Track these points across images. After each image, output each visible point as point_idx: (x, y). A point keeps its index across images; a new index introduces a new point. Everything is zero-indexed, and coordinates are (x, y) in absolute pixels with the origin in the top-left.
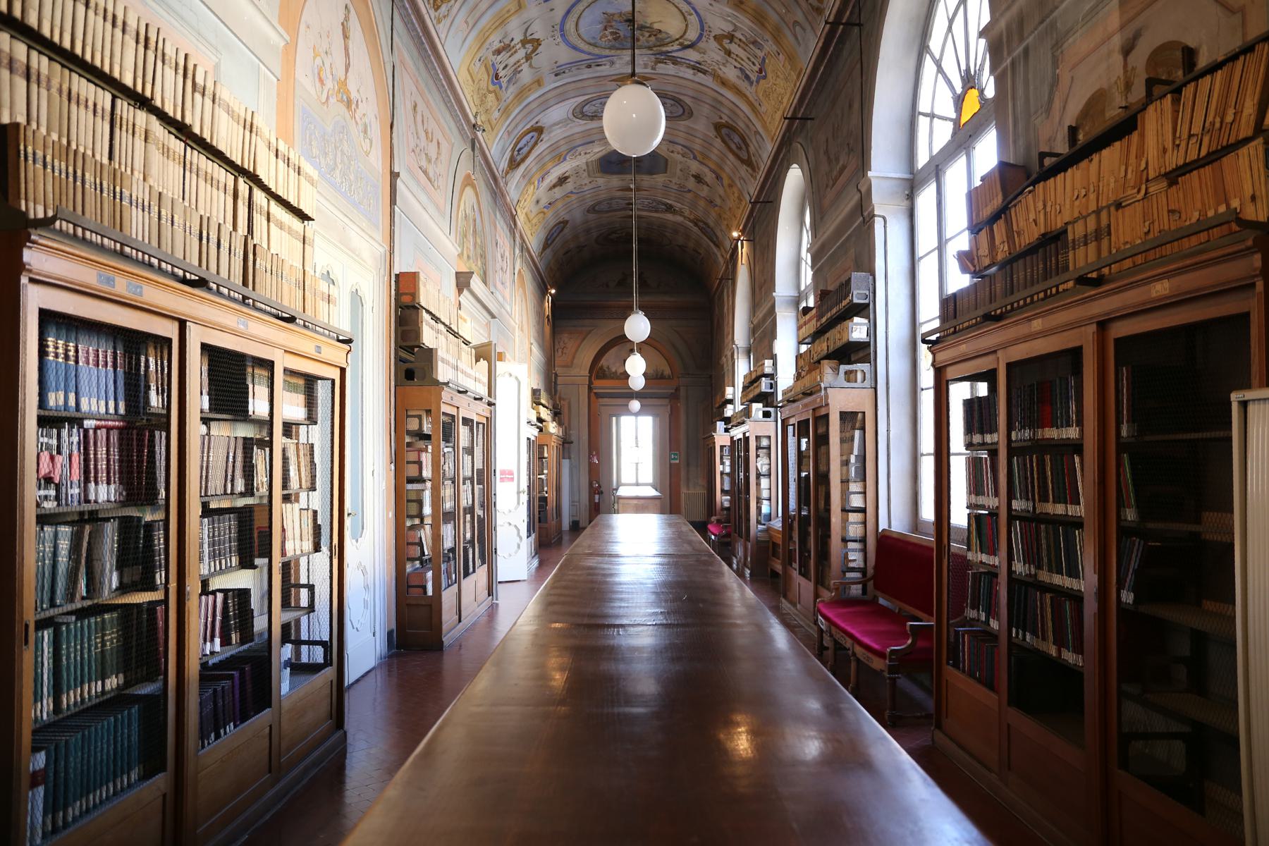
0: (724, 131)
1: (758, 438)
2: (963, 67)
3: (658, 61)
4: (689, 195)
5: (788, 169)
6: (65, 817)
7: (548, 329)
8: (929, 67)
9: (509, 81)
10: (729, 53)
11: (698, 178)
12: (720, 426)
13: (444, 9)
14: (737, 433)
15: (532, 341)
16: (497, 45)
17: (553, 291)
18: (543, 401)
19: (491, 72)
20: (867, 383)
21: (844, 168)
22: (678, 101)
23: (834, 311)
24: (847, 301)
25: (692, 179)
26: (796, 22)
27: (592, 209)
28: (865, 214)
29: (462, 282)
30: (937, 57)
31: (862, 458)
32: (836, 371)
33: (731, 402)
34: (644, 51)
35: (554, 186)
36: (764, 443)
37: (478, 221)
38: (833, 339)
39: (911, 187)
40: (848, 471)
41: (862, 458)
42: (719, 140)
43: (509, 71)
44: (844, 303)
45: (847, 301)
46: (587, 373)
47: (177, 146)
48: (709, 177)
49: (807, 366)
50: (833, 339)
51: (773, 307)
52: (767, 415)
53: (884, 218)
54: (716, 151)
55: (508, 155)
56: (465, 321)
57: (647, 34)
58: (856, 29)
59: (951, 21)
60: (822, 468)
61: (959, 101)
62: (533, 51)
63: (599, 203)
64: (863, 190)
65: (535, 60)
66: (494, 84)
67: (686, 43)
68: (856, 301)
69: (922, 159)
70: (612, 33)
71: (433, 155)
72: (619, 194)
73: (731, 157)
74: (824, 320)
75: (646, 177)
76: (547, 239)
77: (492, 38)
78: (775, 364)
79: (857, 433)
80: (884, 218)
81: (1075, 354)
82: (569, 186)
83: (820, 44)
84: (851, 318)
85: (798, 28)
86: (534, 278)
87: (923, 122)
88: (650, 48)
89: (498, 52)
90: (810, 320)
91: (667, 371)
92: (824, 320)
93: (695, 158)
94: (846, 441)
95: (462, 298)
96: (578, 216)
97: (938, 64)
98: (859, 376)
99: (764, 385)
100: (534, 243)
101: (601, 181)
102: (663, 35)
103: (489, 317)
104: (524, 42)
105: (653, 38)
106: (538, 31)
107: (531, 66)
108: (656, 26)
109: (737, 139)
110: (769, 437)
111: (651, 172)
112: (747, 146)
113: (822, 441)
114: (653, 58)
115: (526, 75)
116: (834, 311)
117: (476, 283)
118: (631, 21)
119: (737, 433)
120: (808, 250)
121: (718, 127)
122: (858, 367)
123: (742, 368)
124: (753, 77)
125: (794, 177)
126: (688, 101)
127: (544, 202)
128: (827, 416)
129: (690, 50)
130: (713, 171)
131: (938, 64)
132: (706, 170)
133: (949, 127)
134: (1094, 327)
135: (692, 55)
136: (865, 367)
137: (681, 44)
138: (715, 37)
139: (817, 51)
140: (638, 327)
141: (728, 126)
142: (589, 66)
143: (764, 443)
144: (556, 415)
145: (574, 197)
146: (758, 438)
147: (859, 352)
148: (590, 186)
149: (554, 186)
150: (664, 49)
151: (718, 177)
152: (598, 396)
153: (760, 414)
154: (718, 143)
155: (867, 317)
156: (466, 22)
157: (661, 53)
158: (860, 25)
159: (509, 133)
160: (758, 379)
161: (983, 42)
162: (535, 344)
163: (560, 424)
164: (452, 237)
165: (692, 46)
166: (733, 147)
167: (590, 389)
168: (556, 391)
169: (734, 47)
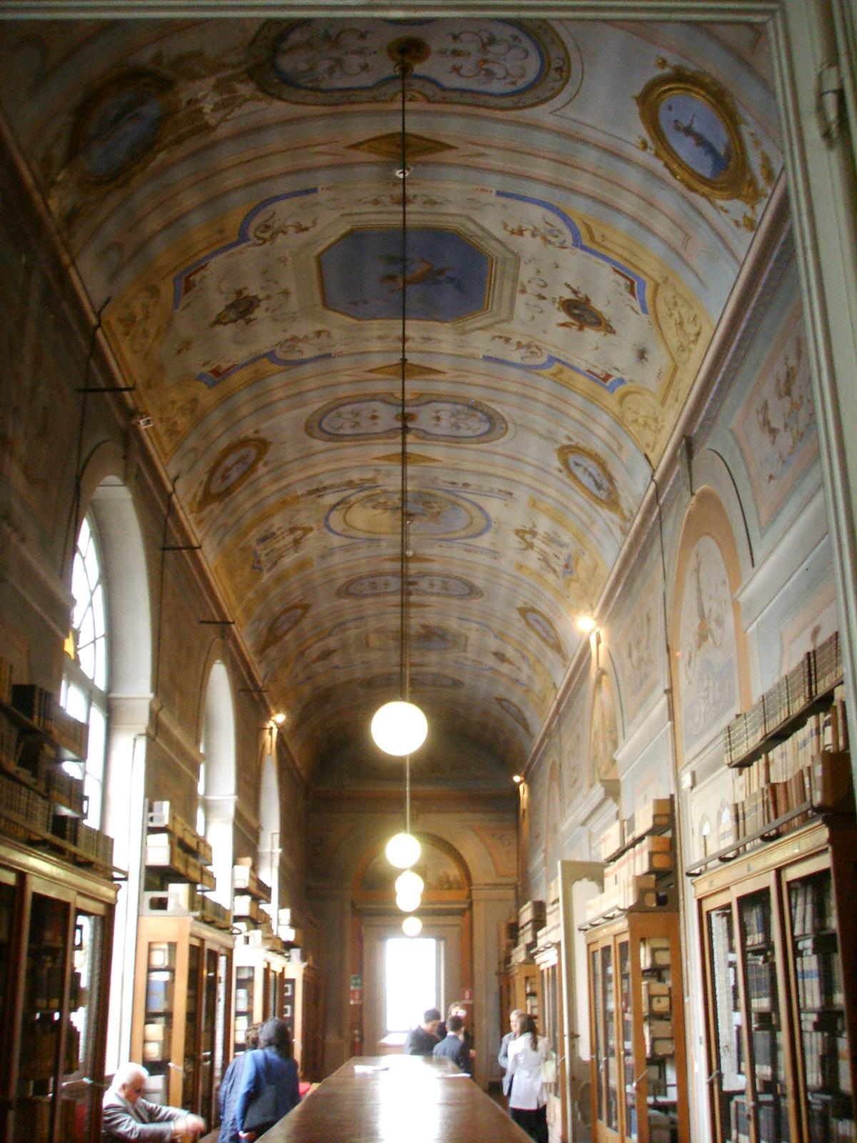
0: (252, 452)
3: (373, 480)
5: (210, 667)
6: (820, 913)
22: (335, 437)
34: (391, 489)
47: (609, 184)
60: (346, 438)
67: (340, 507)
70: (432, 508)
72: (449, 126)
81: (766, 891)
88: (385, 492)
93: (271, 355)
101: (491, 221)
102: (370, 504)
104: (530, 546)
106: (514, 541)
108: (379, 511)
114: (380, 482)
118: (407, 515)
126: (319, 444)
134: (773, 873)
135: (330, 499)
142: (465, 485)
152: (461, 912)
157: (370, 488)
165: (333, 507)
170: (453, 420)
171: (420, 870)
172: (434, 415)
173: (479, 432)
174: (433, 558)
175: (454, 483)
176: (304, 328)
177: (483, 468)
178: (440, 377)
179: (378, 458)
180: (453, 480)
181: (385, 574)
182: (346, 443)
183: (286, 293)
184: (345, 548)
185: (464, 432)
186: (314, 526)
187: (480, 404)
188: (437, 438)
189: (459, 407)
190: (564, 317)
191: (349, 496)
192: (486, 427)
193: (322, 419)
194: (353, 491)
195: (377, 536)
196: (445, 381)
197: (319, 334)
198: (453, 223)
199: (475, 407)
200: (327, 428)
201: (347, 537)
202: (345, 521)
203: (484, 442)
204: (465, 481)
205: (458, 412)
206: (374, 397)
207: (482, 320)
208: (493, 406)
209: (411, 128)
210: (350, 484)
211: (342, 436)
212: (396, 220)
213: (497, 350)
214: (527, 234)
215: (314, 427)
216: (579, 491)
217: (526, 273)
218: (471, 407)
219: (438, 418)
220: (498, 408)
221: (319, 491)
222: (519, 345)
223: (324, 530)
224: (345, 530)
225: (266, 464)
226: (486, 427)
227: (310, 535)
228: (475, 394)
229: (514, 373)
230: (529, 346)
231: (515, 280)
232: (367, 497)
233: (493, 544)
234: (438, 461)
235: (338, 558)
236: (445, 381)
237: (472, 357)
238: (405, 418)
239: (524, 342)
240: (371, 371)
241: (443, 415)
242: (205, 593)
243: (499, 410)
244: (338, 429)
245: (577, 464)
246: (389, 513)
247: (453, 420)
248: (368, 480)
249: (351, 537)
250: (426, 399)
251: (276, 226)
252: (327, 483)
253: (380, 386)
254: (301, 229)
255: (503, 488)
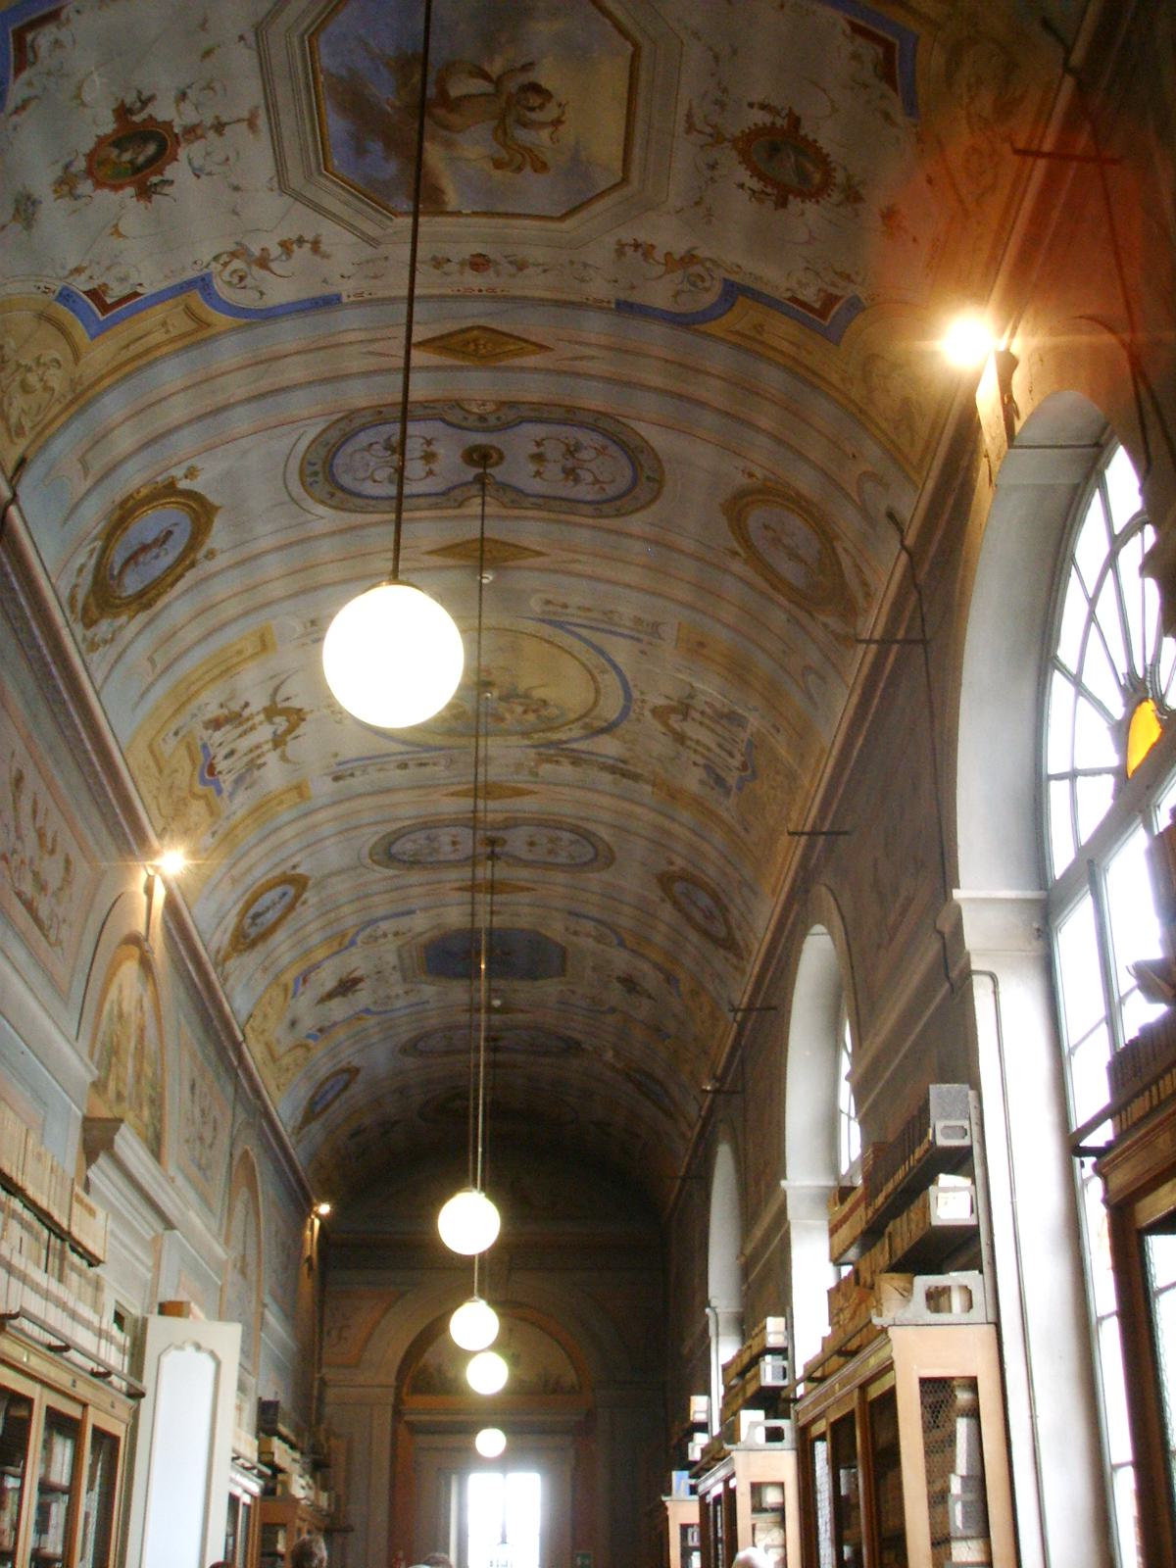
0: (678, 887)
1: (757, 1489)
2: (1122, 668)
4: (610, 1019)
5: (804, 935)
7: (307, 1285)
8: (1059, 685)
9: (239, 781)
10: (680, 738)
11: (630, 983)
12: (680, 1480)
13: (104, 627)
14: (712, 1485)
15: (267, 1299)
16: (213, 711)
17: (325, 1209)
18: (283, 1429)
19: (201, 758)
20: (979, 1312)
21: (909, 901)
22: (584, 835)
23: (900, 1174)
24: (925, 1146)
25: (617, 985)
26: (808, 669)
27: (411, 1048)
28: (954, 974)
29: (97, 1140)
30: (1073, 669)
31: (978, 1481)
32: (907, 1293)
33: (703, 1427)
35: (330, 996)
36: (771, 1497)
37: (151, 1032)
38: (904, 1233)
39: (1044, 912)
40: (946, 1514)
41: (978, 1481)
42: (668, 906)
43: (238, 763)
44: (919, 1152)
45: (925, 1146)
46: (391, 1380)
48: (651, 979)
49: (852, 1299)
50: (904, 1233)
51: (782, 1211)
52: (774, 1435)
53: (993, 977)
54: (663, 928)
55: (231, 921)
56: (92, 1212)
57: (519, 709)
58: (919, 649)
59: (1092, 602)
61: (1122, 731)
62: (289, 731)
63: (426, 1035)
64: (947, 929)
65: (291, 747)
66: (204, 782)
68: (942, 1141)
69: (1062, 858)
71: (54, 880)
73: (694, 937)
74: (880, 1199)
75: (518, 984)
76: (313, 1102)
77: (205, 696)
78: (789, 1327)
79: (962, 1426)
80: (993, 977)
82: (363, 997)
83: (855, 699)
84: (932, 1180)
85: (812, 678)
86: (155, 970)
87: (1058, 792)
88: (525, 734)
89: (216, 724)
90: (852, 1210)
91: (570, 1377)
92: (880, 1199)
93: (622, 943)
94: (939, 1447)
95: (93, 1173)
96: (379, 1059)
97: (1076, 680)
98: (957, 1300)
99: (769, 1373)
100: (285, 1107)
101: (429, 991)
102: (553, 711)
103: (159, 1227)
104: (271, 712)
105: (531, 717)
107: (284, 758)
108: (538, 694)
109: (704, 900)
110: (781, 1485)
111: (532, 975)
112: (725, 910)
113: (886, 1460)
114: (532, 752)
115: (274, 775)
116: (900, 1174)
117: (129, 1145)
119: (712, 1485)
120: (847, 1078)
121: (665, 881)
122: (953, 1279)
123: (724, 1350)
124: (732, 780)
125: (817, 954)
126: (604, 833)
127: (308, 1023)
128: (890, 1395)
129: (605, 739)
130: (658, 967)
131: (1076, 680)
132: (646, 967)
133: (1108, 783)
135: (609, 747)
136: (970, 1278)
137: (585, 726)
138: (654, 711)
139: (850, 712)
140: (469, 1222)
141: (683, 877)
142: (403, 766)
143: (771, 1497)
144: (318, 1467)
145: (372, 1021)
146: (757, 1489)
147: (961, 1248)
148: (413, 999)
149: (330, 996)
150: (556, 736)
151: (670, 979)
152: (414, 1429)
153: (760, 1435)
154: (667, 912)
155: (971, 1174)
156: (151, 660)
157: (550, 744)
158: (924, 642)
159: (235, 881)
160: (755, 1361)
161: (1152, 586)
162: (274, 1307)
163: (324, 1486)
164: (84, 1045)
165: (608, 729)
166: (698, 916)
167: (397, 1413)
168: (320, 1419)
169: (691, 729)
170: (436, 845)
171: (498, 1346)
172: (458, 847)
173: (404, 839)
174: (437, 561)
175: (421, 765)
176: (591, 943)
177: (386, 799)
178: (457, 885)
179: (531, 792)
180: (423, 769)
181: (546, 502)
182: (569, 820)
183: (594, 969)
184: (607, 622)
185: (421, 836)
186: (647, 713)
187: (408, 869)
188: (455, 823)
189: (430, 859)
190: (356, 974)
191: (582, 738)
192: (395, 849)
193: (592, 861)
194: (575, 746)
195: (547, 630)
196: (450, 881)
197: (576, 933)
198: (455, 983)
199: (414, 863)
200: (589, 848)
201: (601, 652)
202: (597, 691)
203: (394, 832)
204: (403, 772)
205: (430, 854)
206: (527, 864)
207: (422, 940)
208: (396, 872)
209: (489, 897)
210: (577, 760)
211: (571, 831)
212: (495, 897)
213: (404, 923)
214: (275, 251)
215: (603, 857)
216: (270, 876)
217: (397, 976)
218: (418, 862)
219: (454, 843)
220: (391, 872)
221: (620, 770)
222: (385, 935)
223: (636, 694)
224: (604, 672)
225: (671, 863)
226: (395, 849)
227: (661, 702)
228: (415, 877)
229: (380, 912)
230: (376, 939)
231: (403, 970)
232: (551, 729)
233: (252, 124)
234: (446, 795)
235: (628, 608)
236: (450, 881)
237: (425, 909)
238: (480, 457)
239: (382, 941)
240: (533, 889)
241: (448, 848)
242: (845, 778)
243: (387, 870)
244: (577, 842)
245: (284, 894)
246: (522, 688)
247: (436, 845)
248: (549, 760)
249: (593, 646)
250: (473, 861)
251: (678, 275)
252: (607, 777)
253: (522, 874)
254: (573, 992)
255: (349, 781)
